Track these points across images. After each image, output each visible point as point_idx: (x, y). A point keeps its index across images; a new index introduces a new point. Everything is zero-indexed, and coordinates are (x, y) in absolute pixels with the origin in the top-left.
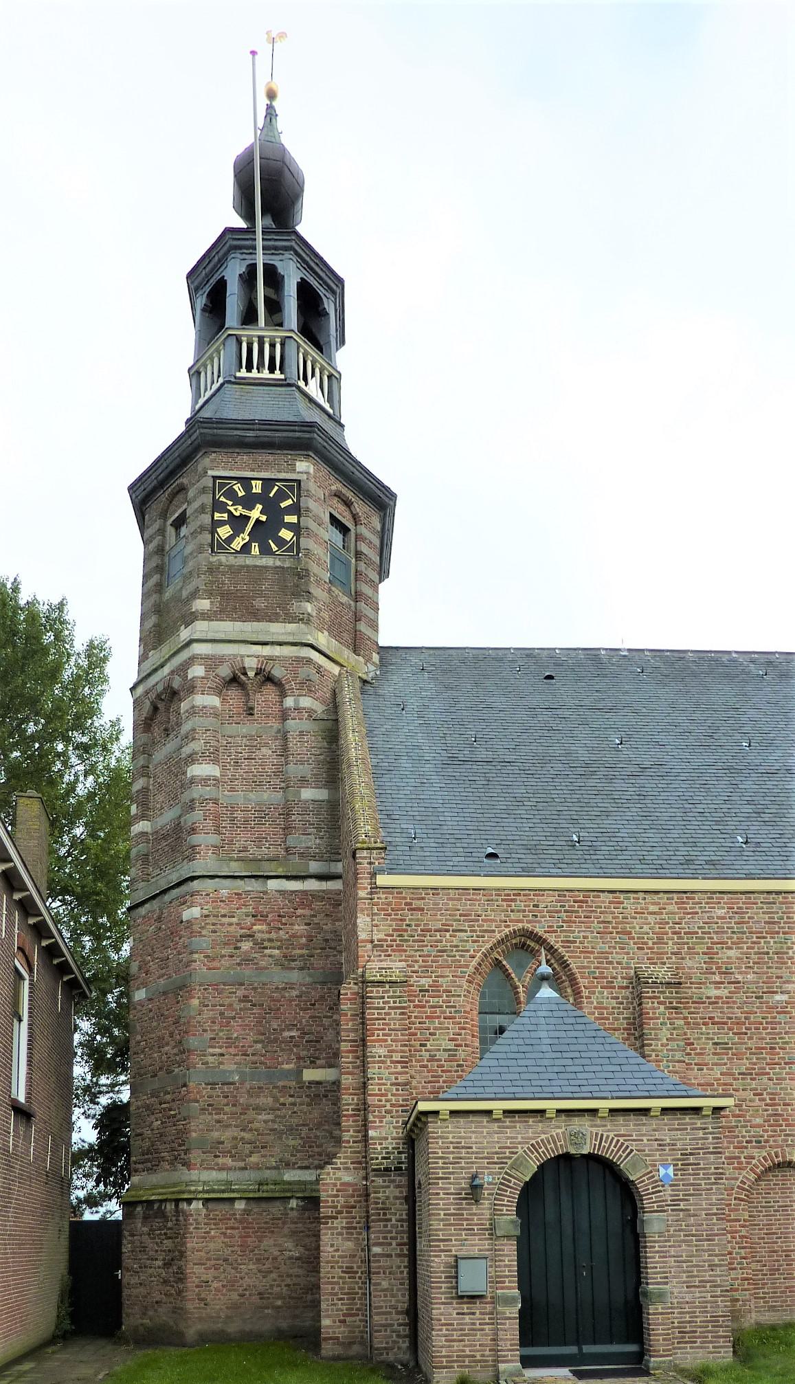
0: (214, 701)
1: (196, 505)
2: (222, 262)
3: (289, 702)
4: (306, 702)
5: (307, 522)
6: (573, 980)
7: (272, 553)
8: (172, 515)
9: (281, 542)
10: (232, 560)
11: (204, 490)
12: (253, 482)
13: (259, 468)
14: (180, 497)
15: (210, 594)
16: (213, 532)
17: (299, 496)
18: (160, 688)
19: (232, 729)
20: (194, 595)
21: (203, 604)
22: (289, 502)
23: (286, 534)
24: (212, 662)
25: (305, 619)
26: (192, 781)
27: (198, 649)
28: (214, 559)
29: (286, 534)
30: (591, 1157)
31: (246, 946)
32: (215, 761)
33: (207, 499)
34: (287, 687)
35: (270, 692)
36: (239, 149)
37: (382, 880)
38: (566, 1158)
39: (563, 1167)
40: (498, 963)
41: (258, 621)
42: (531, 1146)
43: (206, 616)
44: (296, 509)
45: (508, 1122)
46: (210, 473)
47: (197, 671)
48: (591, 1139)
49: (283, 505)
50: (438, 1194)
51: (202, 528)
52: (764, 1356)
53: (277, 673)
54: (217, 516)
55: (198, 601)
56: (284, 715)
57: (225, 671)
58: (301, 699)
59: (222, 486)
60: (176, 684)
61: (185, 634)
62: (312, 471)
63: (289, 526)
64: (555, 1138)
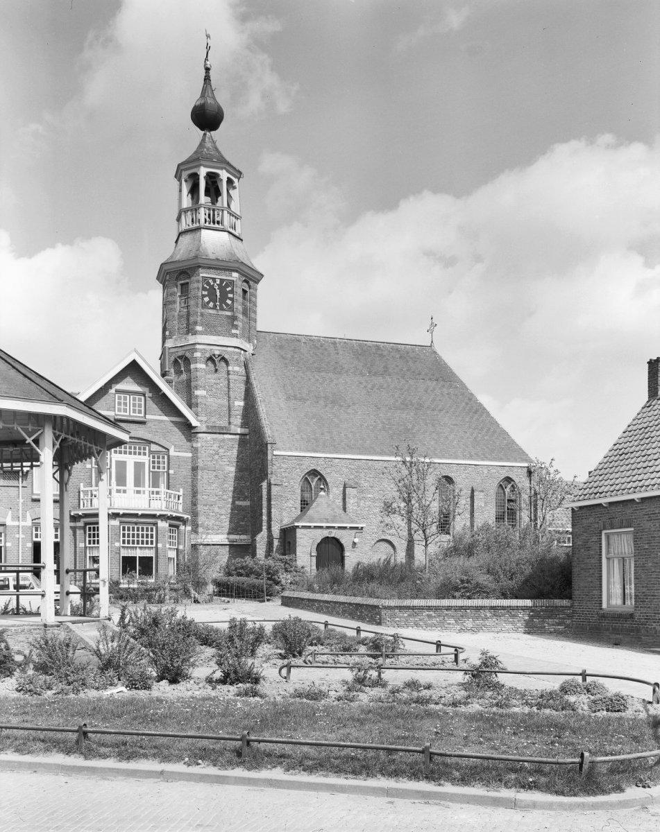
0: (203, 366)
3: (230, 368)
4: (237, 369)
5: (236, 297)
6: (325, 480)
7: (225, 310)
19: (209, 376)
23: (229, 302)
24: (204, 351)
25: (235, 336)
29: (229, 302)
30: (333, 538)
31: (216, 457)
37: (275, 453)
38: (328, 537)
39: (326, 540)
40: (306, 478)
42: (320, 535)
43: (201, 333)
44: (232, 292)
45: (30, 545)
47: (197, 355)
48: (334, 533)
49: (228, 289)
52: (380, 700)
53: (226, 357)
63: (231, 299)
64: (326, 533)
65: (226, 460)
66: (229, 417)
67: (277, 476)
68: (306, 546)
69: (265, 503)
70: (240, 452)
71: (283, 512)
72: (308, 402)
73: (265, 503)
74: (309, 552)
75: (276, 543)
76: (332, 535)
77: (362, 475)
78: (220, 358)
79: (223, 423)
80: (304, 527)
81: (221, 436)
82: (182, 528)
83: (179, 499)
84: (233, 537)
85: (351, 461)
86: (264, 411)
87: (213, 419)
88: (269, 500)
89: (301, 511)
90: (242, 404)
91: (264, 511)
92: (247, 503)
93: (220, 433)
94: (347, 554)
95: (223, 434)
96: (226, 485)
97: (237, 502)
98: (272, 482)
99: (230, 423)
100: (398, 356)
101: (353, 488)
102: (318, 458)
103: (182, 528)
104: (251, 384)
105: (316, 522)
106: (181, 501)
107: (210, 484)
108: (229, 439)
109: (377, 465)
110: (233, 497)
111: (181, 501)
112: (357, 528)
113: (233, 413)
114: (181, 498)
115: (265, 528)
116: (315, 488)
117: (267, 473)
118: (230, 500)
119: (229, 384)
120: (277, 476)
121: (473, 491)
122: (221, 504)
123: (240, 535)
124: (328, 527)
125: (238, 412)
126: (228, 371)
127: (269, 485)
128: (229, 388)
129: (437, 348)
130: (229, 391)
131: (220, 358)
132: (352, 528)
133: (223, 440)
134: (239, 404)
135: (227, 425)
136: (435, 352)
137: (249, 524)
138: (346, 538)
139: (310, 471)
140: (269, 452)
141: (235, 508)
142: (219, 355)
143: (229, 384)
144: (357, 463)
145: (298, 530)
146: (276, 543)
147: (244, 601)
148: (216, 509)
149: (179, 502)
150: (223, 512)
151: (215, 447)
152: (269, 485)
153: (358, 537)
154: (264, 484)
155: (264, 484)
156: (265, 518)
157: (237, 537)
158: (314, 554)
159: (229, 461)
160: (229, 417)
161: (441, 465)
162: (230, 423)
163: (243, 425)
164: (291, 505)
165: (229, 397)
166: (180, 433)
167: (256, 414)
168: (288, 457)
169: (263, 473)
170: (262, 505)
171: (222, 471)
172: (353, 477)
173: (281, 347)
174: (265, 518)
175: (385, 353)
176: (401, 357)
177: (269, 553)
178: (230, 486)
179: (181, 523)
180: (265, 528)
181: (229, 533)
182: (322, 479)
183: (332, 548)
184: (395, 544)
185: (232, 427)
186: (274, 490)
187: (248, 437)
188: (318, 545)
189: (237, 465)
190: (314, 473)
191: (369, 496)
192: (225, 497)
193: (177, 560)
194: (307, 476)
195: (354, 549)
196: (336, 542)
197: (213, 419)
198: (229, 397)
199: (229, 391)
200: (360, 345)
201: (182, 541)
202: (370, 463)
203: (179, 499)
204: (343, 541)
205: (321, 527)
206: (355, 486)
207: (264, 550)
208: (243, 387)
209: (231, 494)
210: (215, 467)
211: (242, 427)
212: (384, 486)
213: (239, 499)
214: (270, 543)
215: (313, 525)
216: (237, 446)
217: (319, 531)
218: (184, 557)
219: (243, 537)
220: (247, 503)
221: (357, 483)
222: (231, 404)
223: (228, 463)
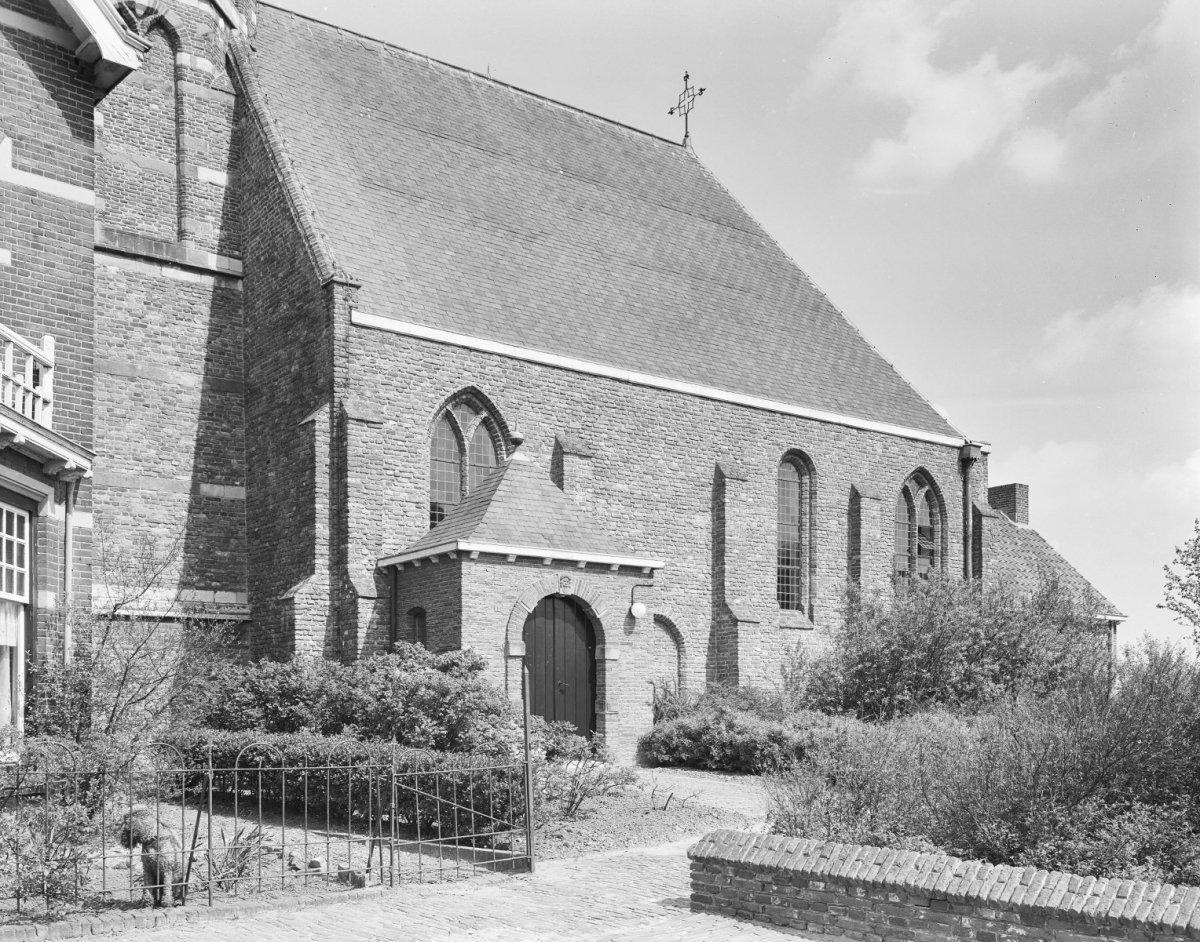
3: (184, 58)
4: (205, 65)
31: (138, 335)
37: (357, 317)
40: (448, 416)
48: (578, 585)
53: (173, 19)
58: (199, 59)
64: (550, 582)
65: (170, 349)
66: (180, 216)
67: (361, 395)
68: (492, 618)
69: (323, 480)
70: (215, 331)
71: (387, 522)
72: (426, 204)
73: (323, 480)
74: (502, 642)
75: (366, 613)
76: (569, 592)
77: (601, 424)
78: (150, 18)
79: (161, 228)
80: (486, 557)
81: (154, 271)
82: (53, 511)
83: (36, 381)
84: (188, 595)
85: (573, 377)
86: (308, 192)
87: (128, 213)
88: (339, 470)
89: (433, 526)
90: (222, 178)
91: (322, 506)
92: (237, 492)
93: (150, 260)
94: (611, 652)
95: (162, 263)
96: (169, 430)
97: (206, 489)
98: (350, 410)
99: (181, 233)
100: (619, 150)
101: (582, 457)
102: (484, 351)
103: (53, 511)
104: (256, 116)
105: (519, 542)
106: (46, 389)
107: (117, 419)
108: (180, 284)
109: (643, 398)
110: (196, 469)
111: (46, 389)
112: (636, 571)
113: (191, 200)
114: (48, 378)
115: (322, 562)
116: (472, 446)
117: (332, 382)
118: (187, 479)
119: (179, 111)
120: (361, 395)
121: (855, 497)
122: (154, 487)
123: (215, 589)
124: (558, 563)
125: (208, 204)
126: (177, 68)
127: (340, 423)
128: (179, 122)
129: (699, 147)
130: (179, 132)
131: (150, 18)
132: (625, 569)
133: (161, 285)
134: (214, 177)
135: (174, 237)
136: (694, 161)
137: (243, 557)
138: (607, 601)
139: (461, 393)
140: (339, 313)
141: (198, 503)
142: (149, 11)
143: (179, 111)
144: (589, 385)
145: (465, 566)
146: (366, 613)
147: (719, 917)
148: (138, 506)
149: (38, 390)
150: (160, 514)
151: (135, 301)
152: (340, 423)
153: (643, 600)
154: (322, 418)
155: (322, 418)
156: (322, 530)
157: (205, 596)
158: (518, 649)
159: (181, 355)
160: (180, 216)
161: (787, 420)
162: (181, 233)
163: (229, 245)
164: (403, 496)
165: (179, 151)
166: (43, 92)
167: (284, 210)
168: (399, 335)
169: (315, 382)
170: (312, 485)
171: (159, 383)
172: (577, 425)
173: (326, 54)
174: (322, 530)
175: (589, 135)
176: (626, 153)
177: (340, 647)
178: (185, 430)
179: (49, 490)
180: (322, 562)
181: (184, 584)
182: (494, 424)
183: (568, 632)
184: (682, 629)
185: (190, 245)
186: (356, 435)
187: (239, 286)
188: (531, 617)
189: (207, 371)
190: (472, 399)
191: (619, 486)
192: (167, 467)
193: (31, 655)
194: (449, 407)
195: (631, 638)
196: (579, 612)
197: (128, 213)
198: (179, 151)
199: (179, 132)
200: (527, 103)
201: (52, 574)
202: (623, 389)
203: (36, 381)
204: (601, 611)
205: (536, 561)
206: (589, 452)
207: (321, 636)
208: (224, 129)
209: (187, 460)
210: (134, 368)
211: (220, 253)
212: (656, 461)
213: (211, 478)
214: (342, 614)
215: (513, 550)
216: (205, 310)
217: (530, 572)
218: (60, 647)
219: (224, 597)
220: (237, 492)
221: (588, 446)
222: (186, 172)
223: (177, 359)
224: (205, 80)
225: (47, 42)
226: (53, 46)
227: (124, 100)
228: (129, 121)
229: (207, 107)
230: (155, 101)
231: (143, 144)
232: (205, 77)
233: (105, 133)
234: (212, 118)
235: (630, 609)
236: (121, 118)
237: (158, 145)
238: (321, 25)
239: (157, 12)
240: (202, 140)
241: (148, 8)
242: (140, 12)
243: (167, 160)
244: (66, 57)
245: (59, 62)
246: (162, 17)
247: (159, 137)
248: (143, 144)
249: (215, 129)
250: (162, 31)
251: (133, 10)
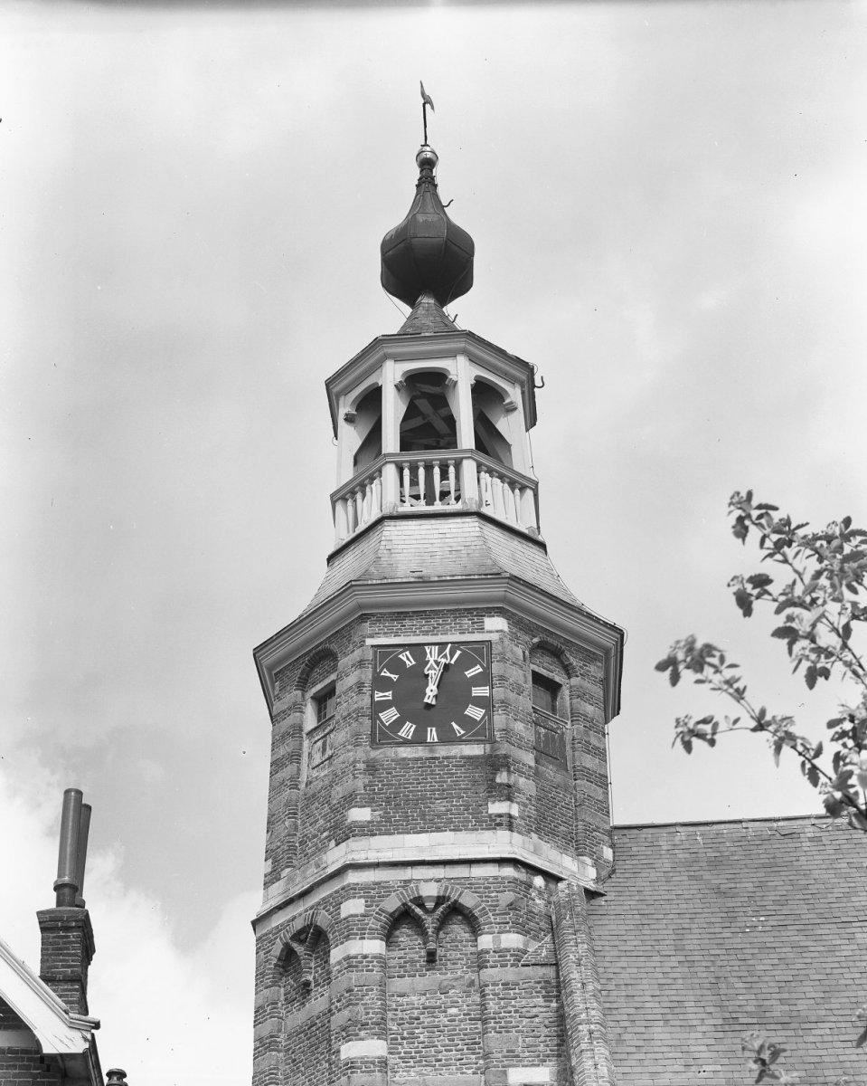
1: (351, 680)
2: (378, 365)
3: (485, 941)
8: (314, 684)
9: (467, 723)
10: (405, 752)
11: (361, 664)
12: (427, 649)
13: (433, 631)
14: (327, 664)
15: (369, 802)
16: (374, 717)
17: (490, 662)
18: (299, 924)
20: (350, 800)
21: (360, 814)
22: (478, 669)
24: (372, 893)
26: (351, 1066)
27: (353, 878)
28: (374, 754)
29: (475, 713)
32: (382, 1033)
33: (367, 675)
34: (481, 920)
35: (458, 930)
36: (513, 449)
41: (439, 830)
43: (367, 830)
46: (369, 642)
49: (469, 673)
50: (509, 882)
51: (359, 713)
53: (468, 900)
54: (379, 696)
55: (353, 810)
56: (480, 962)
57: (392, 904)
58: (503, 936)
59: (384, 656)
60: (323, 919)
61: (336, 856)
62: (506, 628)
224: (512, 958)
225: (10, 1050)
226: (16, 1052)
227: (415, 1015)
228: (422, 1039)
229: (517, 991)
230: (454, 1004)
231: (440, 1060)
232: (512, 955)
233: (391, 1062)
234: (524, 1002)
235: (791, 564)
236: (413, 1037)
237: (459, 1057)
238: (715, 827)
239: (449, 898)
240: (513, 1034)
241: (438, 897)
242: (430, 905)
243: (470, 1071)
244: (30, 1060)
245: (21, 1067)
246: (456, 901)
247: (460, 1047)
248: (440, 1060)
249: (528, 1015)
250: (460, 917)
251: (421, 906)
